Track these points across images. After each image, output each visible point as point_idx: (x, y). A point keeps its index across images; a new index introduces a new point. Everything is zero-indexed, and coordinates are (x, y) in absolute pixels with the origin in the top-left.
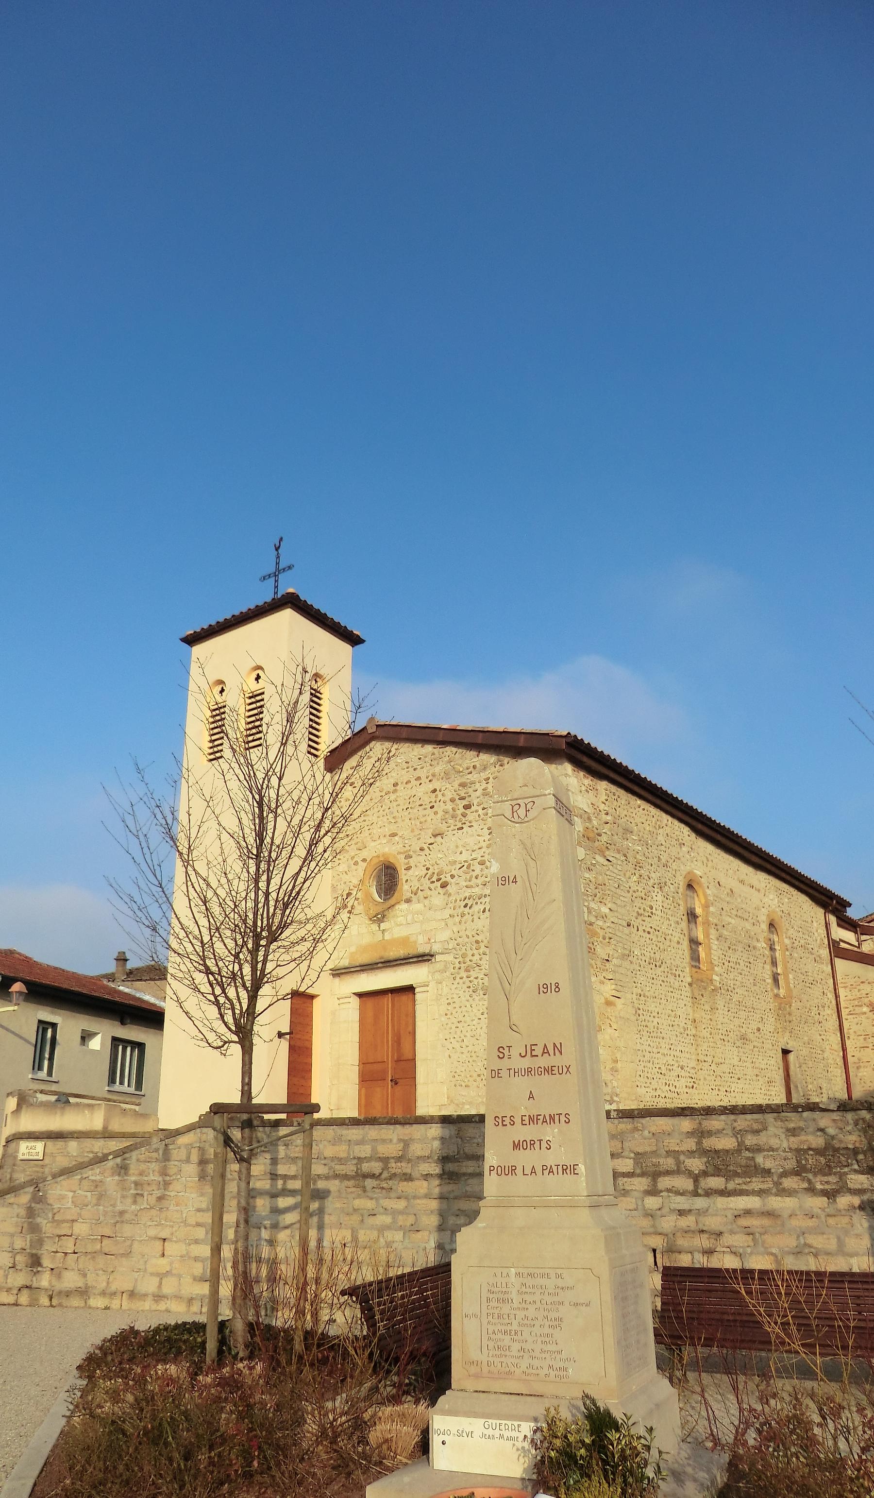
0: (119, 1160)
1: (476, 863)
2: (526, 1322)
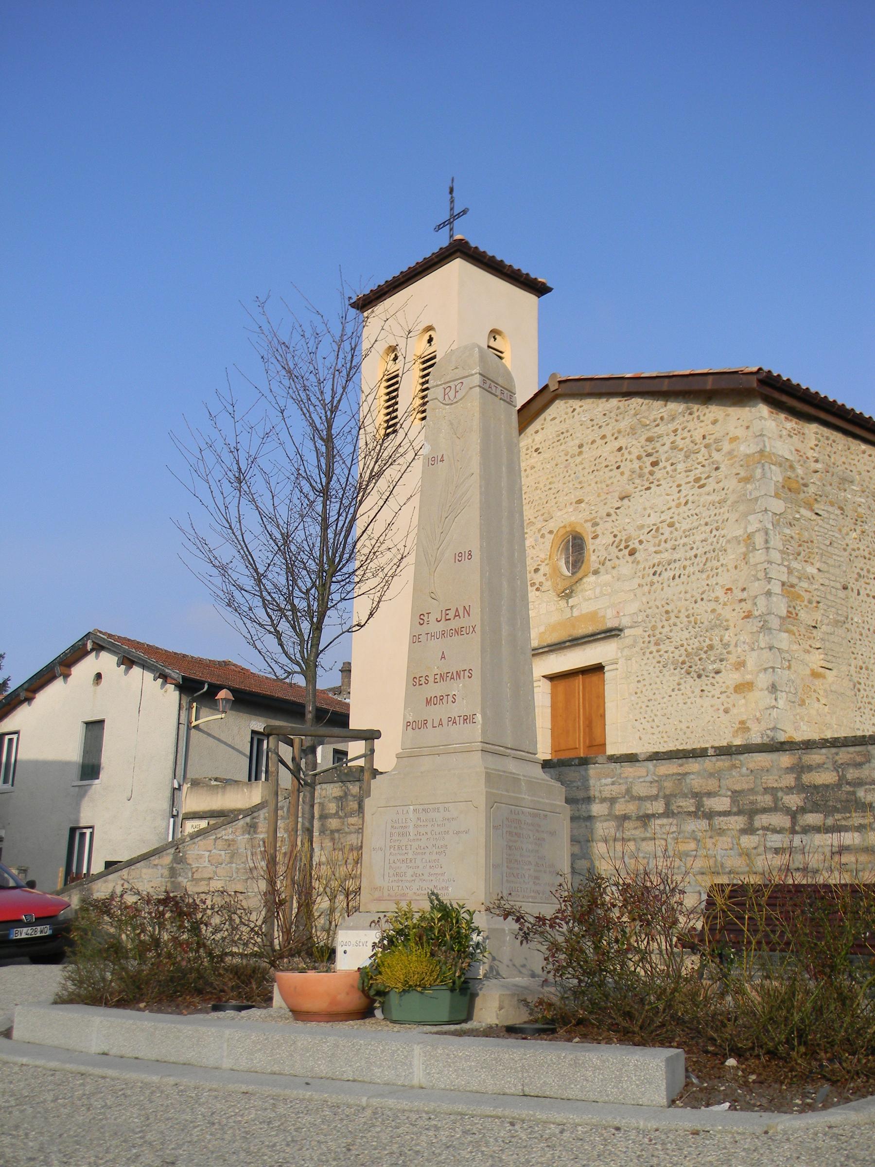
0: (248, 819)
1: (665, 525)
2: (419, 851)
